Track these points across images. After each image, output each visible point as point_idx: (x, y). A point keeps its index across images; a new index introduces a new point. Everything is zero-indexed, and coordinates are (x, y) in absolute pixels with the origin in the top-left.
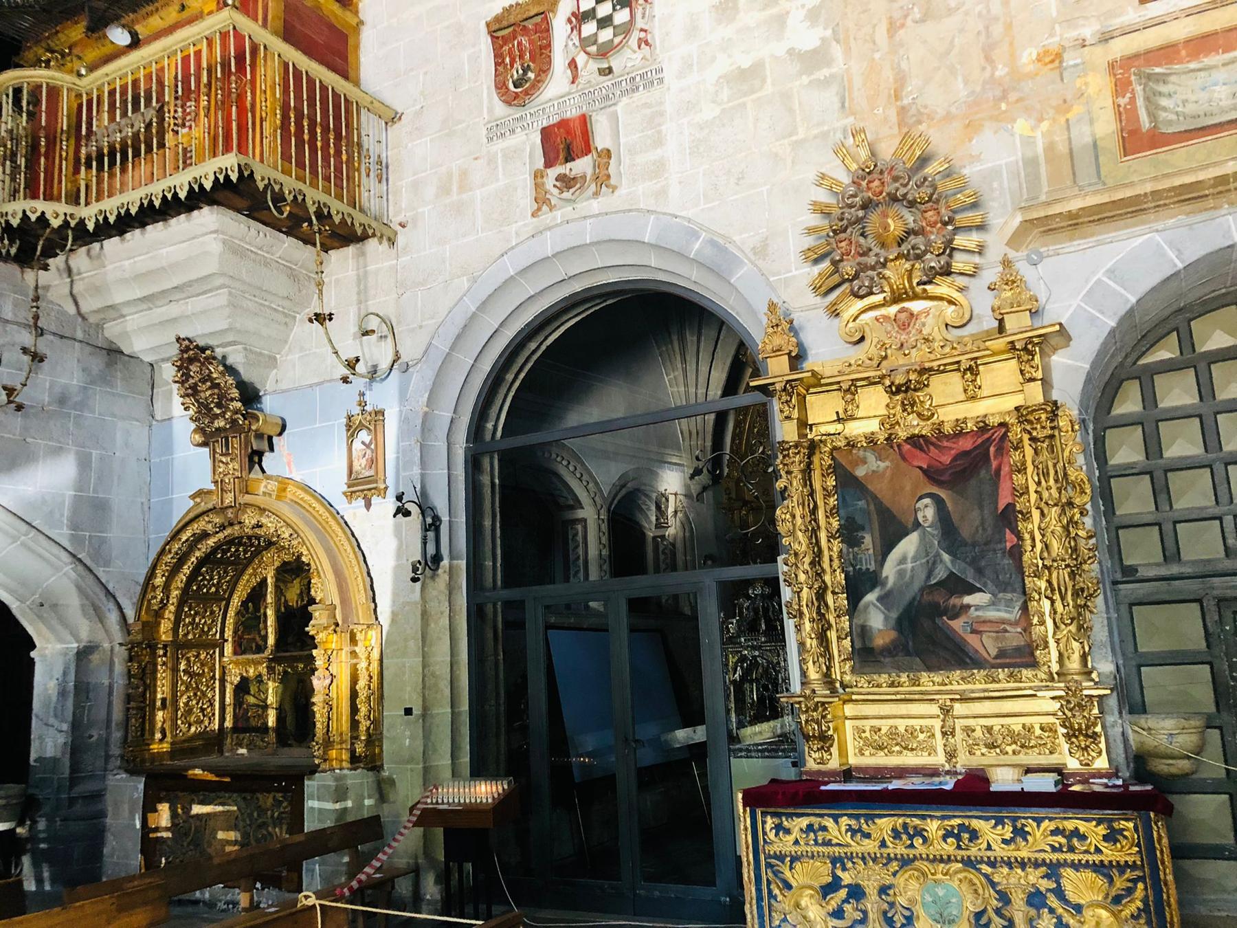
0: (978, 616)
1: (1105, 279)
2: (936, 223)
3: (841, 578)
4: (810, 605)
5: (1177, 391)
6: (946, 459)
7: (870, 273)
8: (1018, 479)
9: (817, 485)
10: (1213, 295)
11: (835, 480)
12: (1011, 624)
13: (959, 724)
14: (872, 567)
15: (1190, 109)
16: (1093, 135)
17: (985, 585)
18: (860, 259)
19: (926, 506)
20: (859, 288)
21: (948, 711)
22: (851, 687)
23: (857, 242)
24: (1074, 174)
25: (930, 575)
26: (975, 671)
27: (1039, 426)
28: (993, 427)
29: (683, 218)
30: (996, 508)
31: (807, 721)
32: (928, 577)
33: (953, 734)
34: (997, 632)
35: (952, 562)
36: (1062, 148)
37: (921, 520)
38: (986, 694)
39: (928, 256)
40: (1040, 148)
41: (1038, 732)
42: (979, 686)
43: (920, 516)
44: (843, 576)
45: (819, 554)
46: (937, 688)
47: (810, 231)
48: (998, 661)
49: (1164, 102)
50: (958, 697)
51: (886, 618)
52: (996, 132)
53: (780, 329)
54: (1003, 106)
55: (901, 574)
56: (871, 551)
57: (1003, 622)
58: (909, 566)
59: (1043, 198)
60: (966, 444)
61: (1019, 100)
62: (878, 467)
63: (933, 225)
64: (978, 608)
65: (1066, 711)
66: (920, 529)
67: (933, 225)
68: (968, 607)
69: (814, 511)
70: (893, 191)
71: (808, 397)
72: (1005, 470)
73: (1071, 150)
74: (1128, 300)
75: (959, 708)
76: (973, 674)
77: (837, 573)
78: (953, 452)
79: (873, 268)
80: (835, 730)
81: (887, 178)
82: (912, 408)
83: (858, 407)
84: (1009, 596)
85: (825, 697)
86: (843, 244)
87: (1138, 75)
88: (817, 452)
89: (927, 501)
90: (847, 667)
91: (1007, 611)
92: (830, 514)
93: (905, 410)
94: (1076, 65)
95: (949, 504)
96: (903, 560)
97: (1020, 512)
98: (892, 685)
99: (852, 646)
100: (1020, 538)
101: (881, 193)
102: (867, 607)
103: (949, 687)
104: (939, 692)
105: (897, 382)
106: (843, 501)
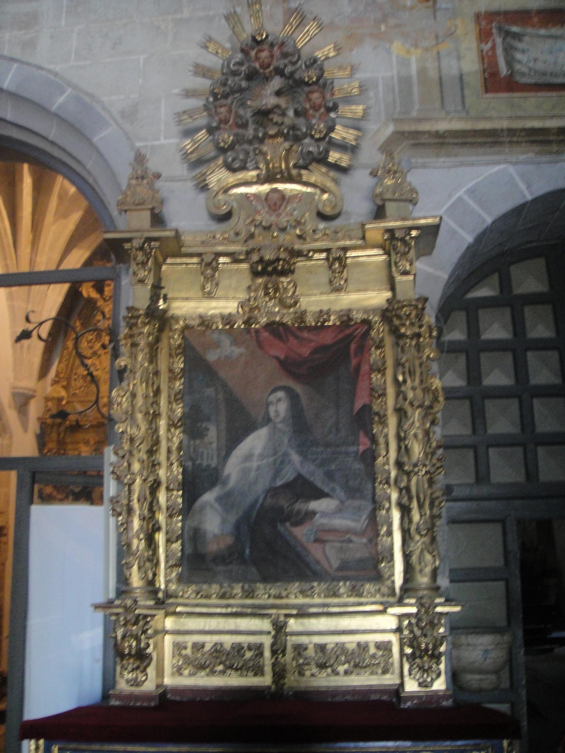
0: (322, 524)
1: (466, 197)
2: (320, 107)
3: (177, 470)
4: (142, 500)
5: (496, 326)
6: (305, 351)
7: (246, 146)
8: (376, 377)
9: (163, 366)
10: (529, 246)
11: (184, 362)
12: (356, 533)
13: (292, 640)
14: (214, 463)
15: (540, 66)
16: (460, 69)
17: (333, 490)
18: (236, 130)
19: (279, 400)
20: (234, 160)
21: (281, 627)
22: (176, 597)
23: (236, 112)
24: (442, 98)
25: (277, 472)
26: (315, 584)
27: (408, 323)
28: (356, 323)
29: (49, 71)
30: (352, 409)
31: (124, 637)
32: (274, 479)
33: (284, 652)
34: (342, 542)
35: (302, 462)
36: (433, 74)
37: (272, 414)
38: (325, 610)
39: (307, 141)
40: (414, 69)
41: (372, 650)
42: (317, 600)
43: (272, 409)
44: (181, 470)
45: (157, 442)
46: (271, 601)
47: (189, 94)
48: (340, 574)
49: (519, 56)
50: (294, 612)
51: (224, 521)
52: (375, 48)
53: (145, 181)
54: (383, 28)
55: (245, 472)
56: (214, 445)
57: (348, 531)
58: (255, 464)
59: (414, 114)
60: (328, 338)
61: (397, 26)
62: (233, 352)
63: (316, 108)
64: (324, 514)
65: (416, 629)
66: (271, 425)
67: (316, 108)
68: (314, 513)
69: (157, 392)
70: (282, 66)
71: (164, 268)
72: (365, 368)
73: (440, 78)
74: (484, 221)
75: (293, 624)
76: (313, 587)
77: (175, 465)
78: (313, 344)
79: (250, 142)
80: (155, 647)
81: (276, 51)
82: (275, 293)
83: (217, 285)
84: (357, 503)
85: (150, 608)
86: (223, 110)
87: (500, 29)
88: (167, 330)
89: (281, 394)
90: (174, 574)
91: (354, 520)
92: (177, 397)
93: (267, 294)
94: (447, 9)
95: (304, 400)
96: (248, 457)
97: (377, 414)
98: (223, 596)
99: (182, 550)
100: (374, 440)
101: (269, 65)
102: (202, 508)
103: (284, 601)
104: (273, 607)
105: (267, 257)
106: (189, 387)
